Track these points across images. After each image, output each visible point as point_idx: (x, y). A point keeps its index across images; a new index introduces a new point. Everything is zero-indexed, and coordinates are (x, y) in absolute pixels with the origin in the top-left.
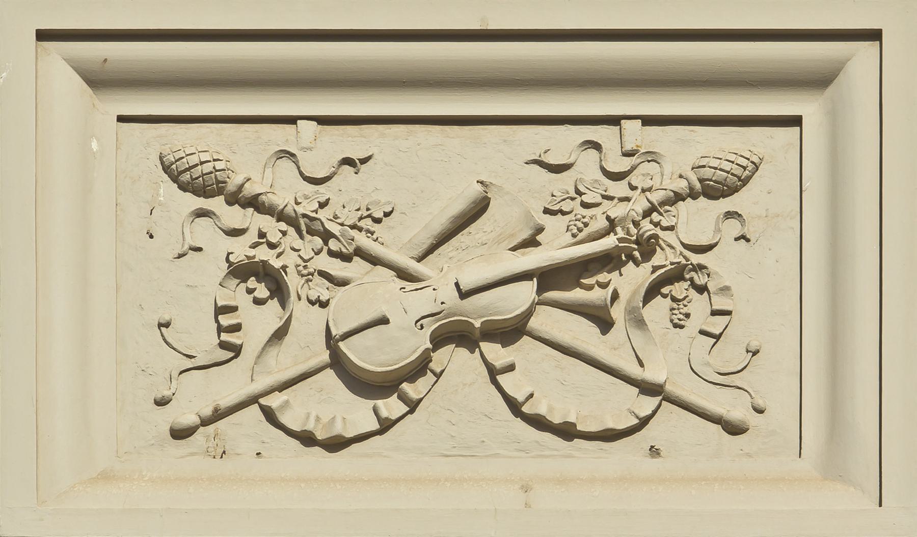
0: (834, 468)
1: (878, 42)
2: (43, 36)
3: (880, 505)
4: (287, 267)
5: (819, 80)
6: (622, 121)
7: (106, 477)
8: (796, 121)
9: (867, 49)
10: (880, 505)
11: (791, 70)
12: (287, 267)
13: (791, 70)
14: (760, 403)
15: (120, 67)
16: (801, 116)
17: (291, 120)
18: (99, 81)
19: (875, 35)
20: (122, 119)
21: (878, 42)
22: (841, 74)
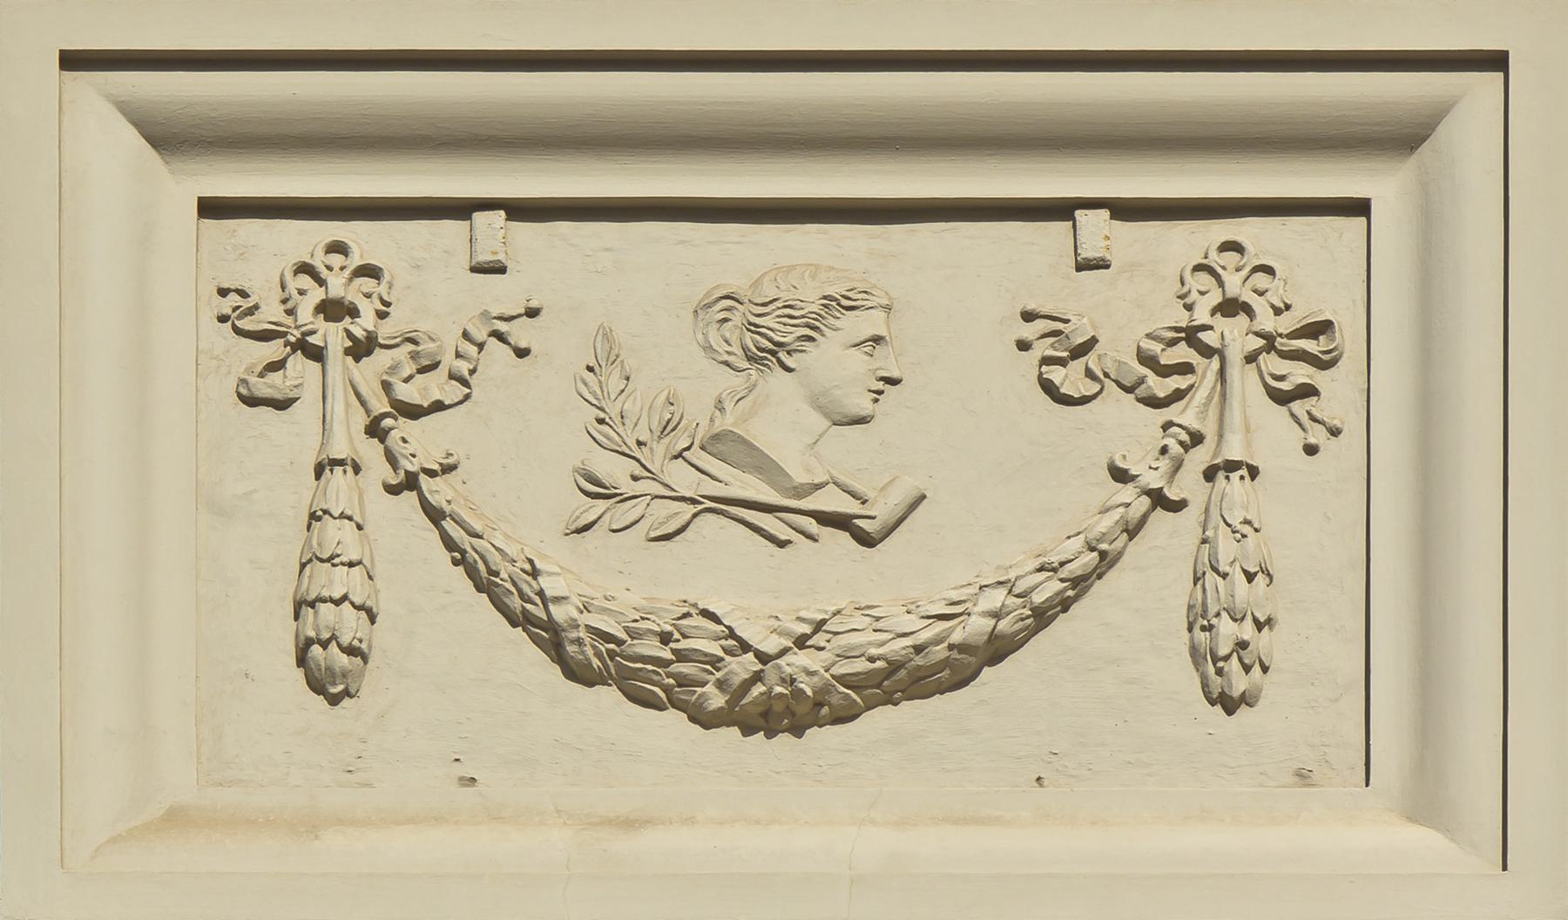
0: (1426, 802)
1: (1501, 74)
2: (72, 61)
3: (1505, 868)
4: (347, 352)
5: (1402, 138)
6: (1078, 213)
7: (176, 819)
8: (1359, 207)
9: (1491, 81)
10: (1505, 868)
11: (1362, 117)
12: (347, 352)
13: (1362, 117)
14: (523, 345)
15: (208, 116)
16: (1369, 200)
17: (461, 209)
18: (169, 138)
19: (1496, 61)
20: (211, 208)
21: (1501, 74)
22: (1440, 128)
